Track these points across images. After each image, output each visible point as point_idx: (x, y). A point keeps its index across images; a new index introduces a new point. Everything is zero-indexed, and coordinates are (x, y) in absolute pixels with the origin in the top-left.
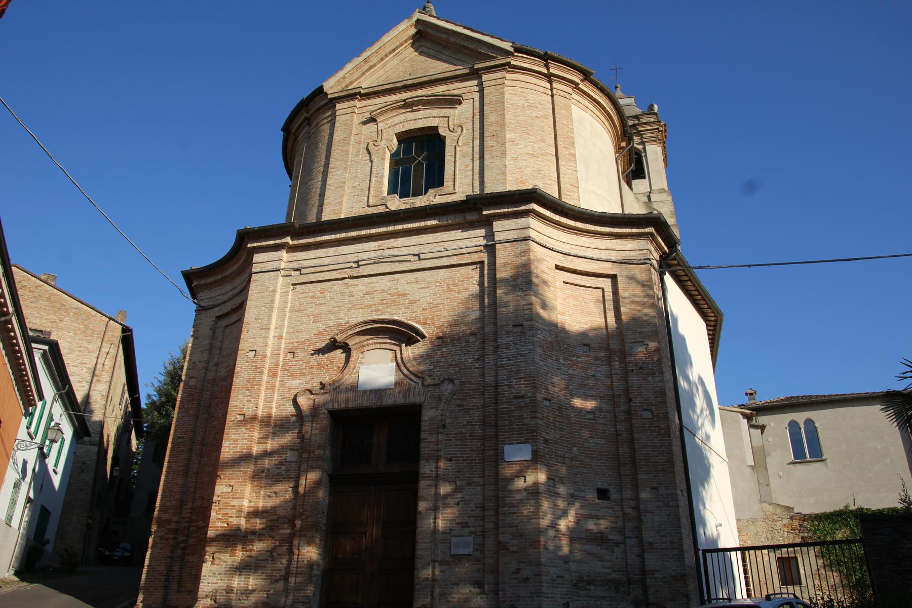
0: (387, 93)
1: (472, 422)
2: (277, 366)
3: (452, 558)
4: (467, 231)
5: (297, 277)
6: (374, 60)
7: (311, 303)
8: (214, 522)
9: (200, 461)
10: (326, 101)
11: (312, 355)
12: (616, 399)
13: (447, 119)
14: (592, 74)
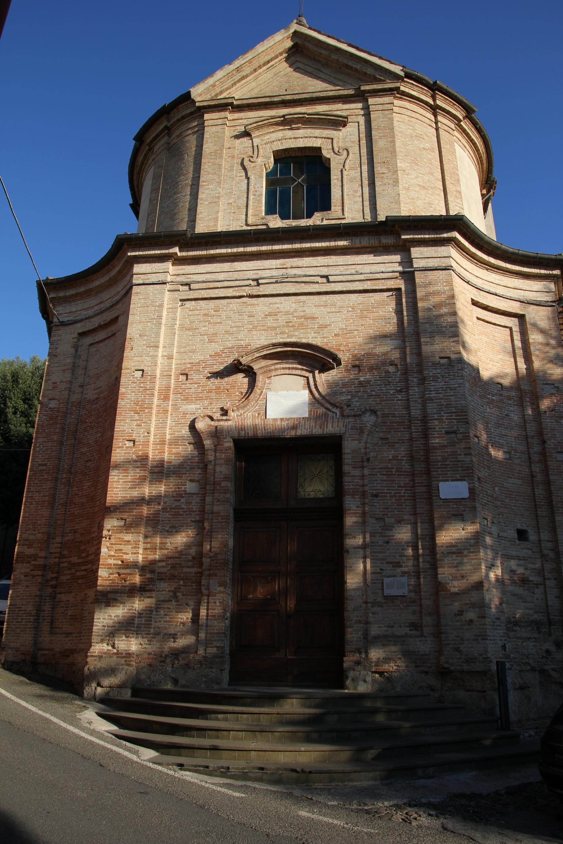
0: (262, 107)
1: (398, 457)
2: (168, 388)
3: (384, 599)
4: (380, 256)
5: (185, 293)
6: (247, 70)
7: (204, 321)
8: (106, 559)
9: (68, 491)
10: (192, 109)
11: (208, 378)
12: (530, 440)
13: (330, 140)
14: (474, 111)
